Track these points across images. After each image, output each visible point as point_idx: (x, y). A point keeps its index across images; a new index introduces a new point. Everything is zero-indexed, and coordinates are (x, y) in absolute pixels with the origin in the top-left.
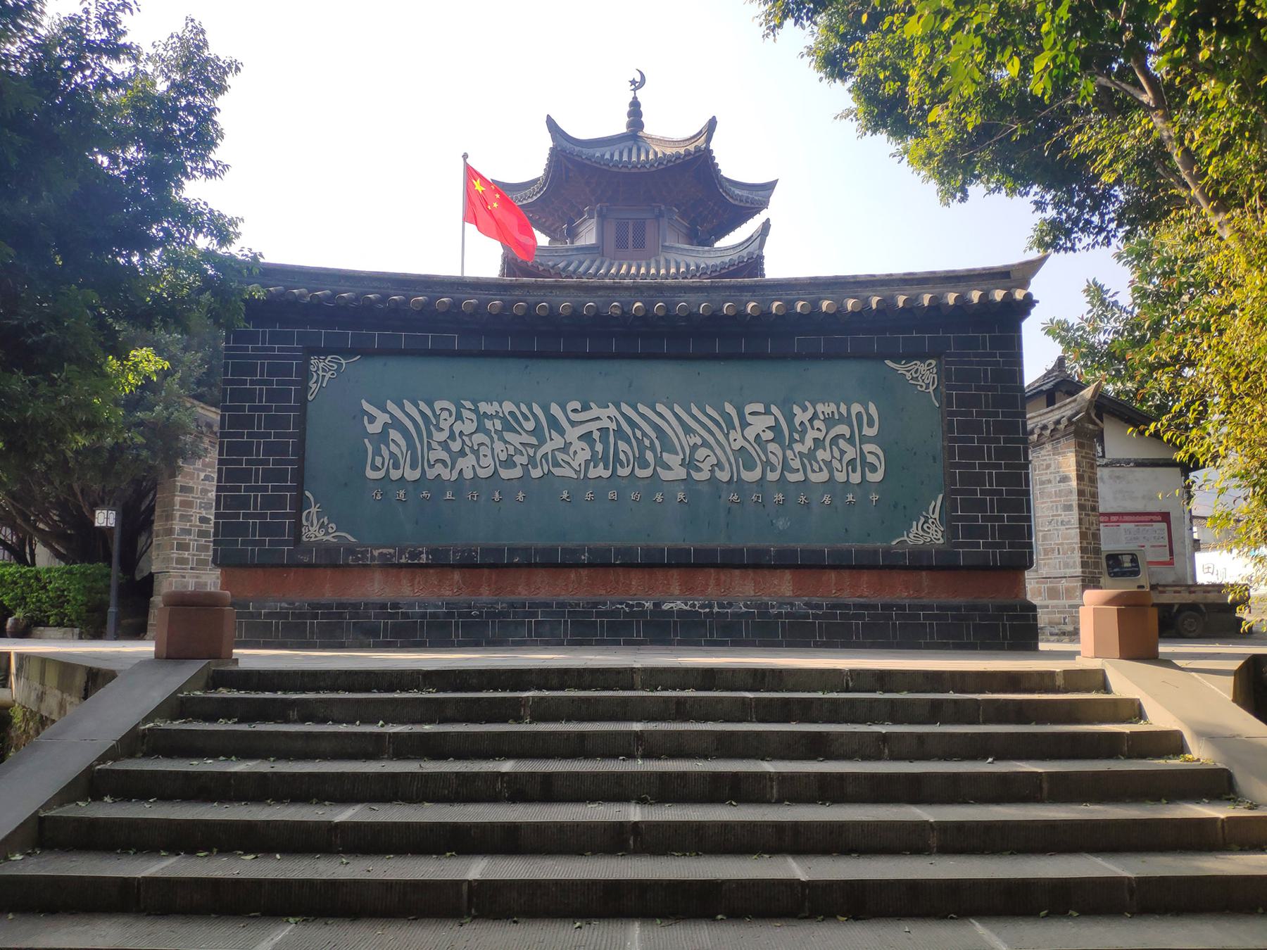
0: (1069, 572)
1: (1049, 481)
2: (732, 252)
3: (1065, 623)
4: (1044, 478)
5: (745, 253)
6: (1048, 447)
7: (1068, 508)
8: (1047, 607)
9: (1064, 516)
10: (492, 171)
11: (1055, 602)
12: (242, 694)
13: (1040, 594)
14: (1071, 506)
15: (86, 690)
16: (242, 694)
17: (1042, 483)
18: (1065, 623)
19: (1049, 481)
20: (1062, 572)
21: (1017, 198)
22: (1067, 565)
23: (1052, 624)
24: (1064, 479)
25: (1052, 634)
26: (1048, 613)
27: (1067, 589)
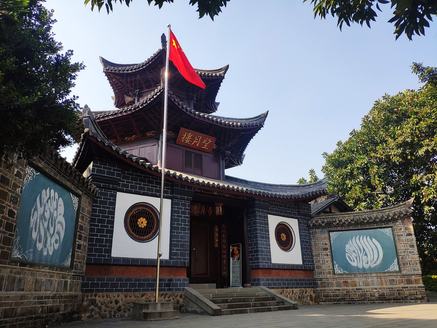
0: (416, 272)
1: (402, 235)
2: (245, 121)
3: (417, 294)
4: (399, 234)
5: (255, 122)
6: (400, 221)
7: (412, 246)
8: (407, 288)
9: (411, 249)
10: (80, 74)
11: (411, 285)
12: (164, 130)
13: (403, 282)
14: (413, 245)
15: (266, 116)
16: (164, 130)
17: (399, 236)
18: (417, 294)
19: (402, 235)
20: (413, 272)
21: (361, 122)
22: (414, 270)
23: (410, 295)
24: (410, 235)
25: (411, 299)
26: (408, 290)
27: (415, 280)
